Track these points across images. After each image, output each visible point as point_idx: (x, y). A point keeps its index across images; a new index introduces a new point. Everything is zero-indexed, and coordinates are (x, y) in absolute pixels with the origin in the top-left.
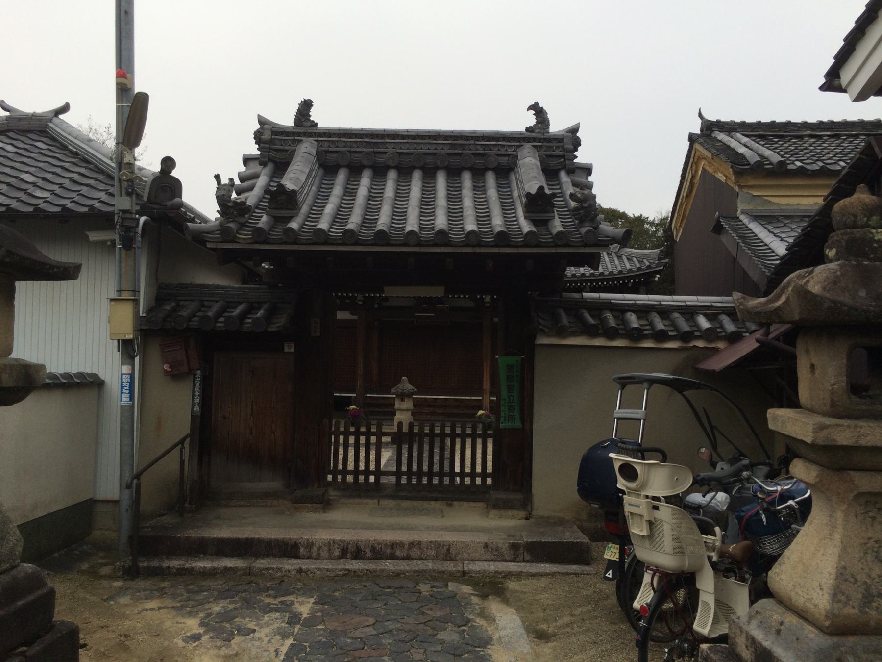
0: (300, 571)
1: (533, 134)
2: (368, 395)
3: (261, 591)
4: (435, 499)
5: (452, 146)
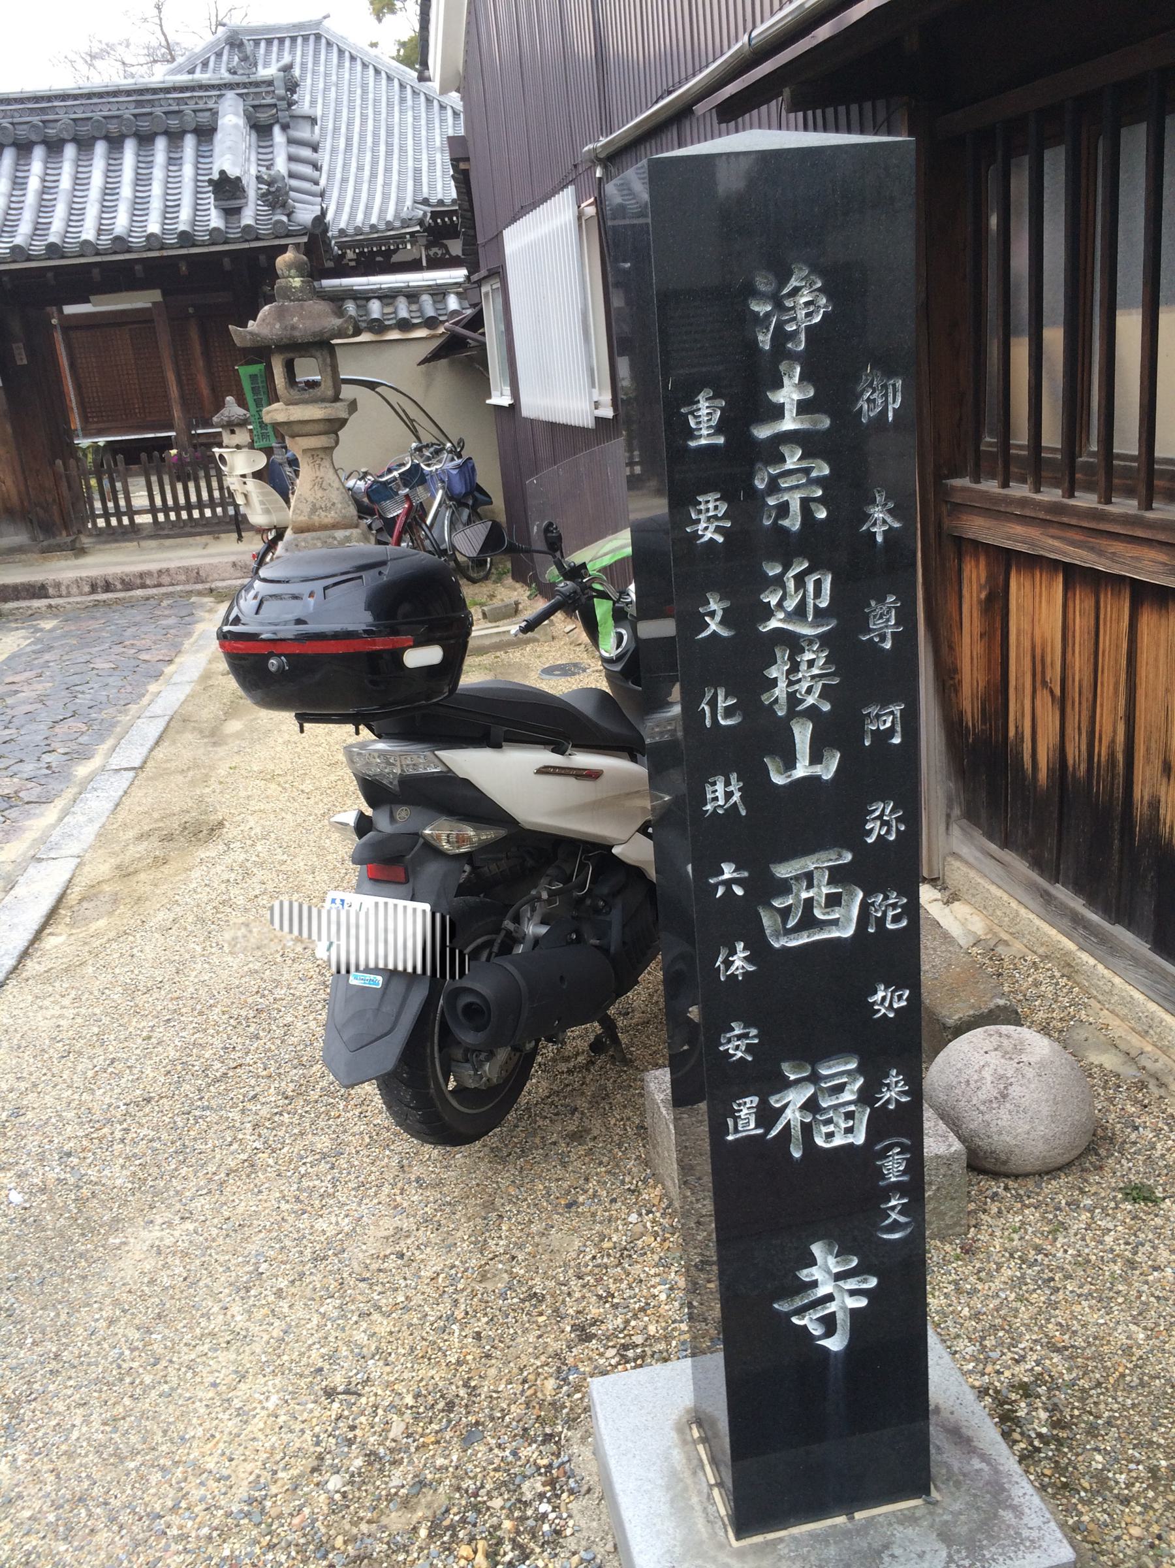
0: (50, 606)
1: (236, 77)
2: (199, 431)
3: (10, 621)
4: (200, 534)
5: (139, 104)
